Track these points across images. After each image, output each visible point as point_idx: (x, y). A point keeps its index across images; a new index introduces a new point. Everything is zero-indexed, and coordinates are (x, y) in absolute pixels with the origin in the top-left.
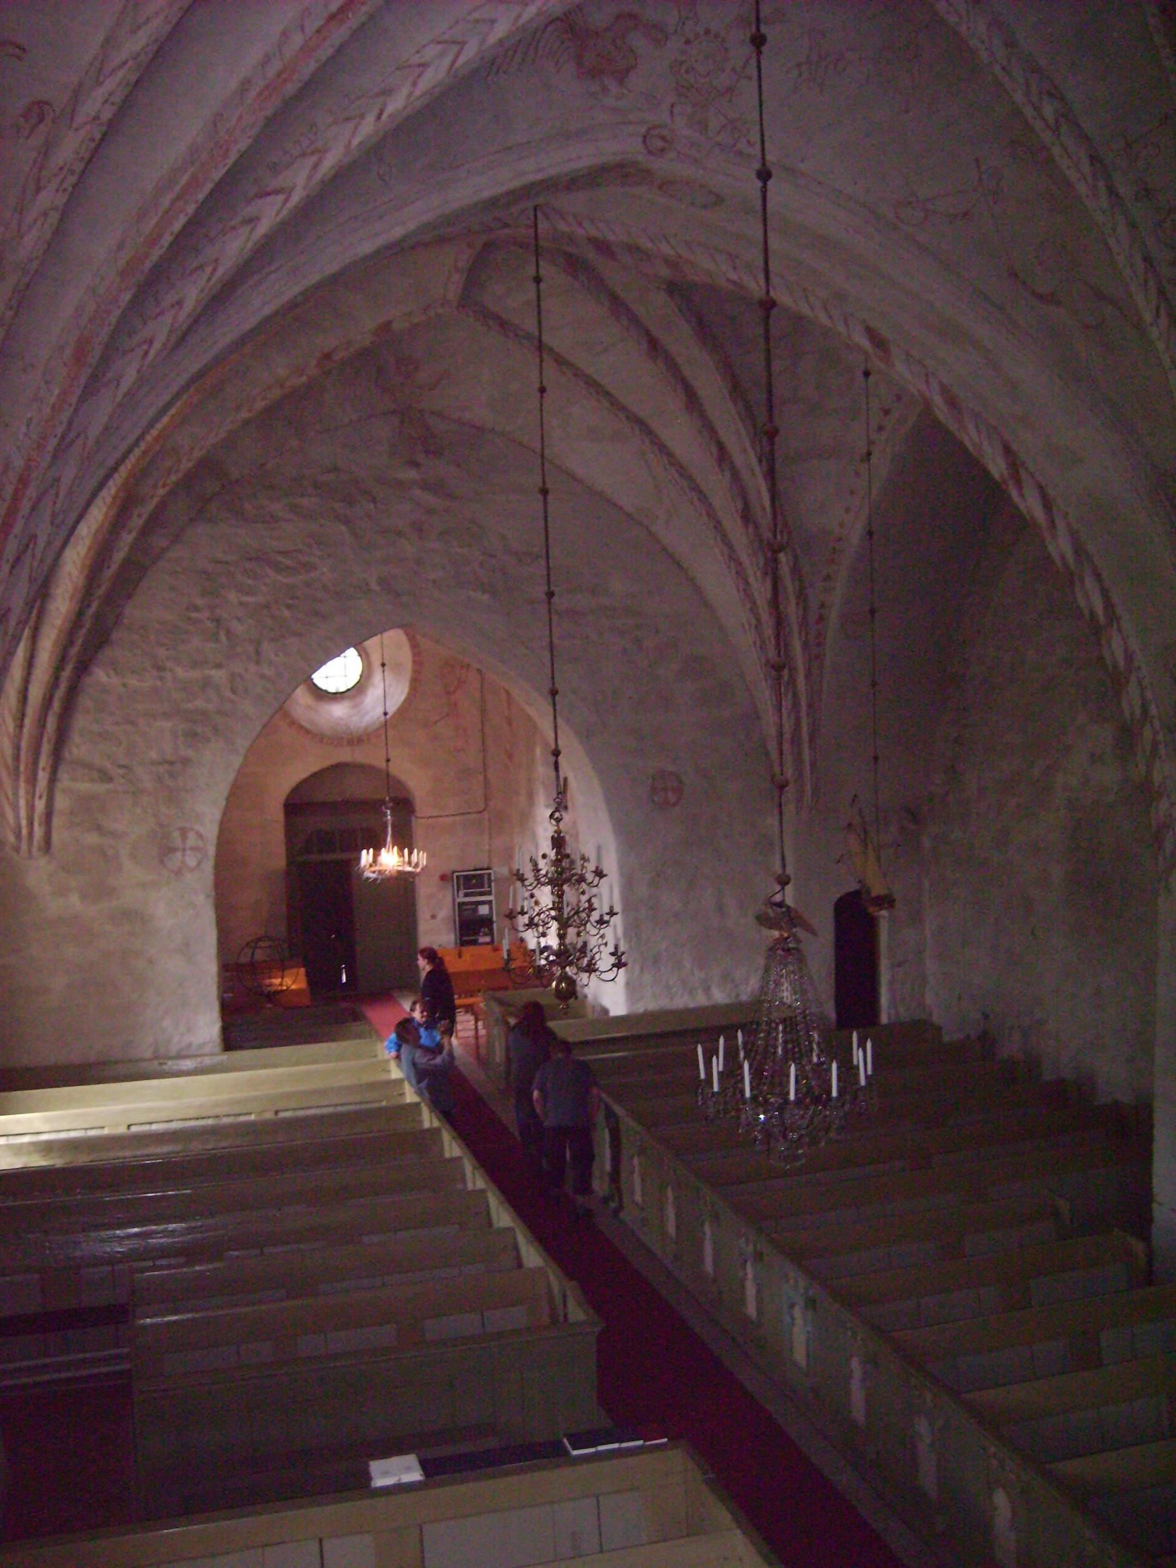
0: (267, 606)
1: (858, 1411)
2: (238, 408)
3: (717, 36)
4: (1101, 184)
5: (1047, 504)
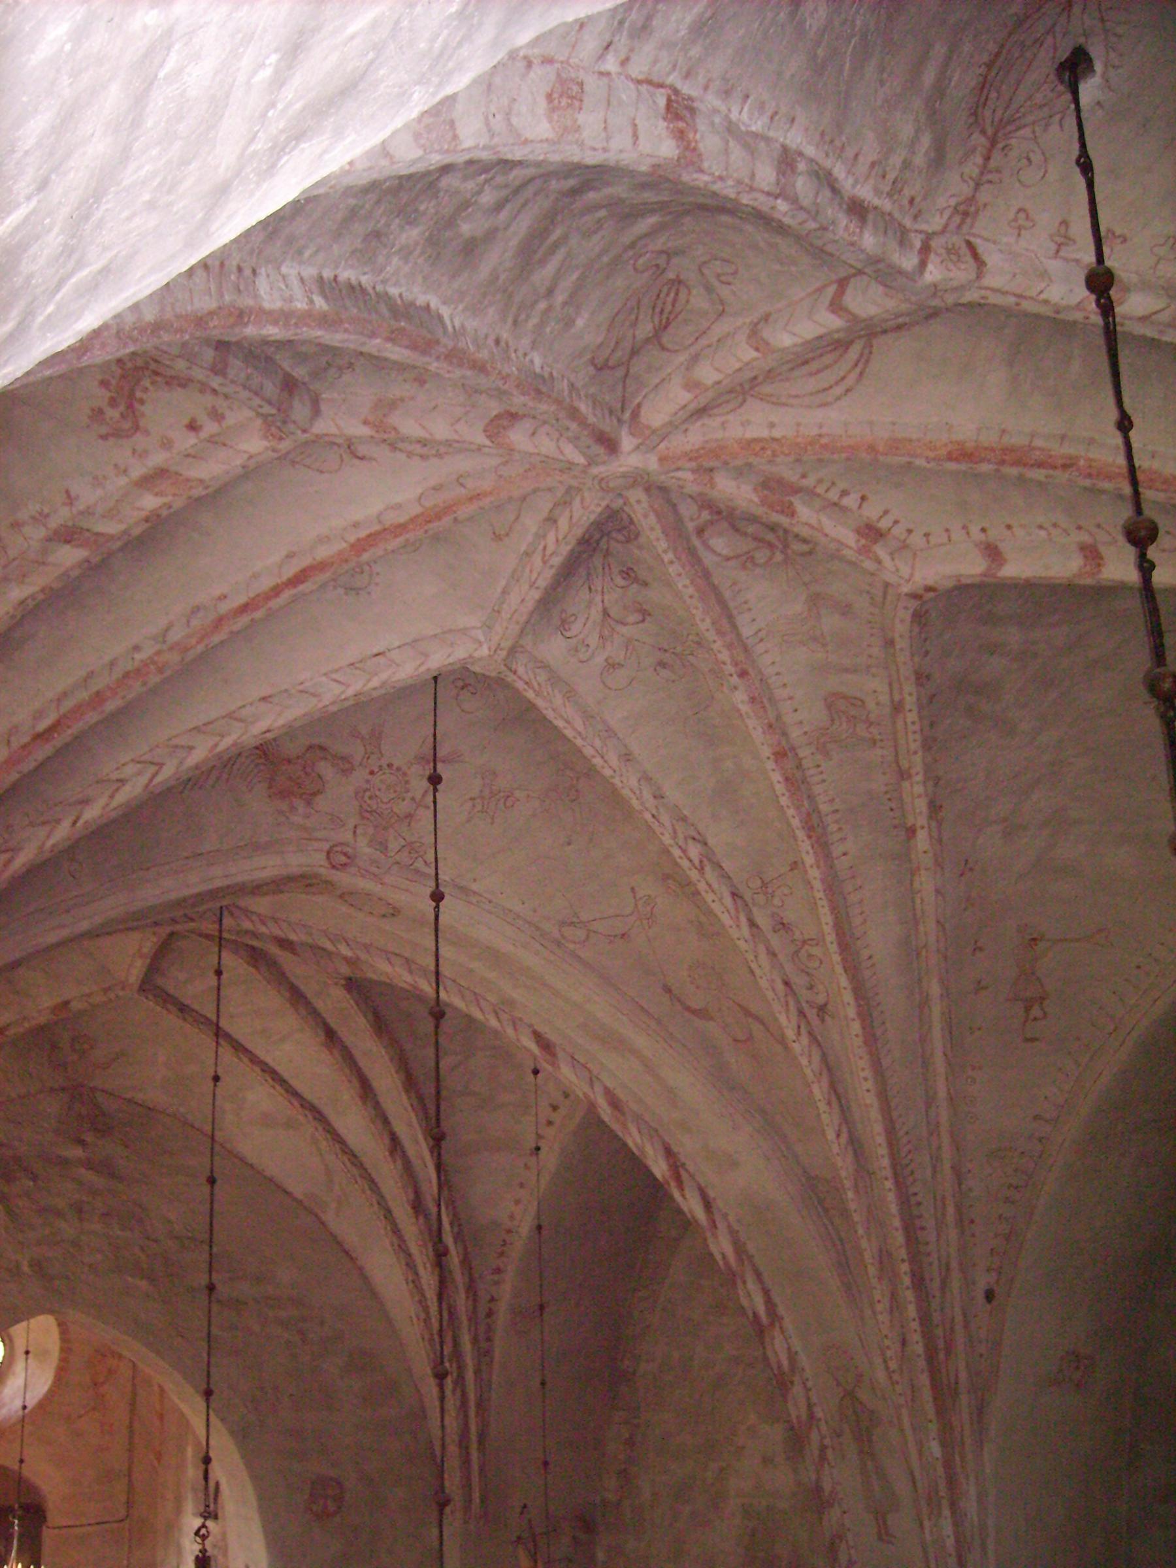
3: (398, 769)
5: (708, 1205)
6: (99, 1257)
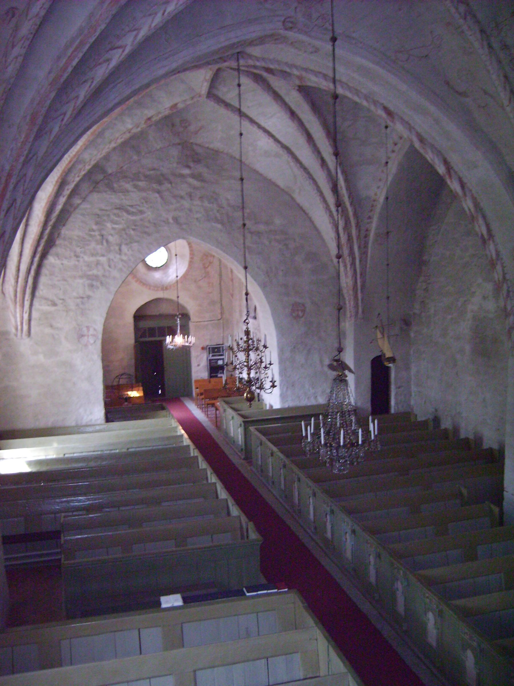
0: (124, 230)
1: (373, 580)
2: (110, 143)
4: (485, 44)
5: (463, 185)
6: (200, 215)
